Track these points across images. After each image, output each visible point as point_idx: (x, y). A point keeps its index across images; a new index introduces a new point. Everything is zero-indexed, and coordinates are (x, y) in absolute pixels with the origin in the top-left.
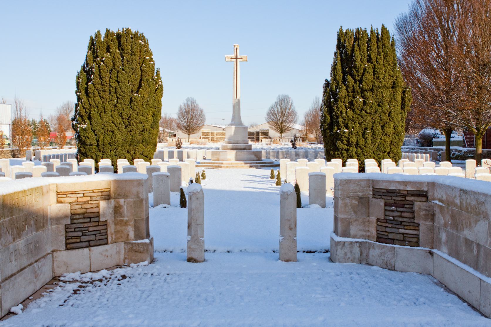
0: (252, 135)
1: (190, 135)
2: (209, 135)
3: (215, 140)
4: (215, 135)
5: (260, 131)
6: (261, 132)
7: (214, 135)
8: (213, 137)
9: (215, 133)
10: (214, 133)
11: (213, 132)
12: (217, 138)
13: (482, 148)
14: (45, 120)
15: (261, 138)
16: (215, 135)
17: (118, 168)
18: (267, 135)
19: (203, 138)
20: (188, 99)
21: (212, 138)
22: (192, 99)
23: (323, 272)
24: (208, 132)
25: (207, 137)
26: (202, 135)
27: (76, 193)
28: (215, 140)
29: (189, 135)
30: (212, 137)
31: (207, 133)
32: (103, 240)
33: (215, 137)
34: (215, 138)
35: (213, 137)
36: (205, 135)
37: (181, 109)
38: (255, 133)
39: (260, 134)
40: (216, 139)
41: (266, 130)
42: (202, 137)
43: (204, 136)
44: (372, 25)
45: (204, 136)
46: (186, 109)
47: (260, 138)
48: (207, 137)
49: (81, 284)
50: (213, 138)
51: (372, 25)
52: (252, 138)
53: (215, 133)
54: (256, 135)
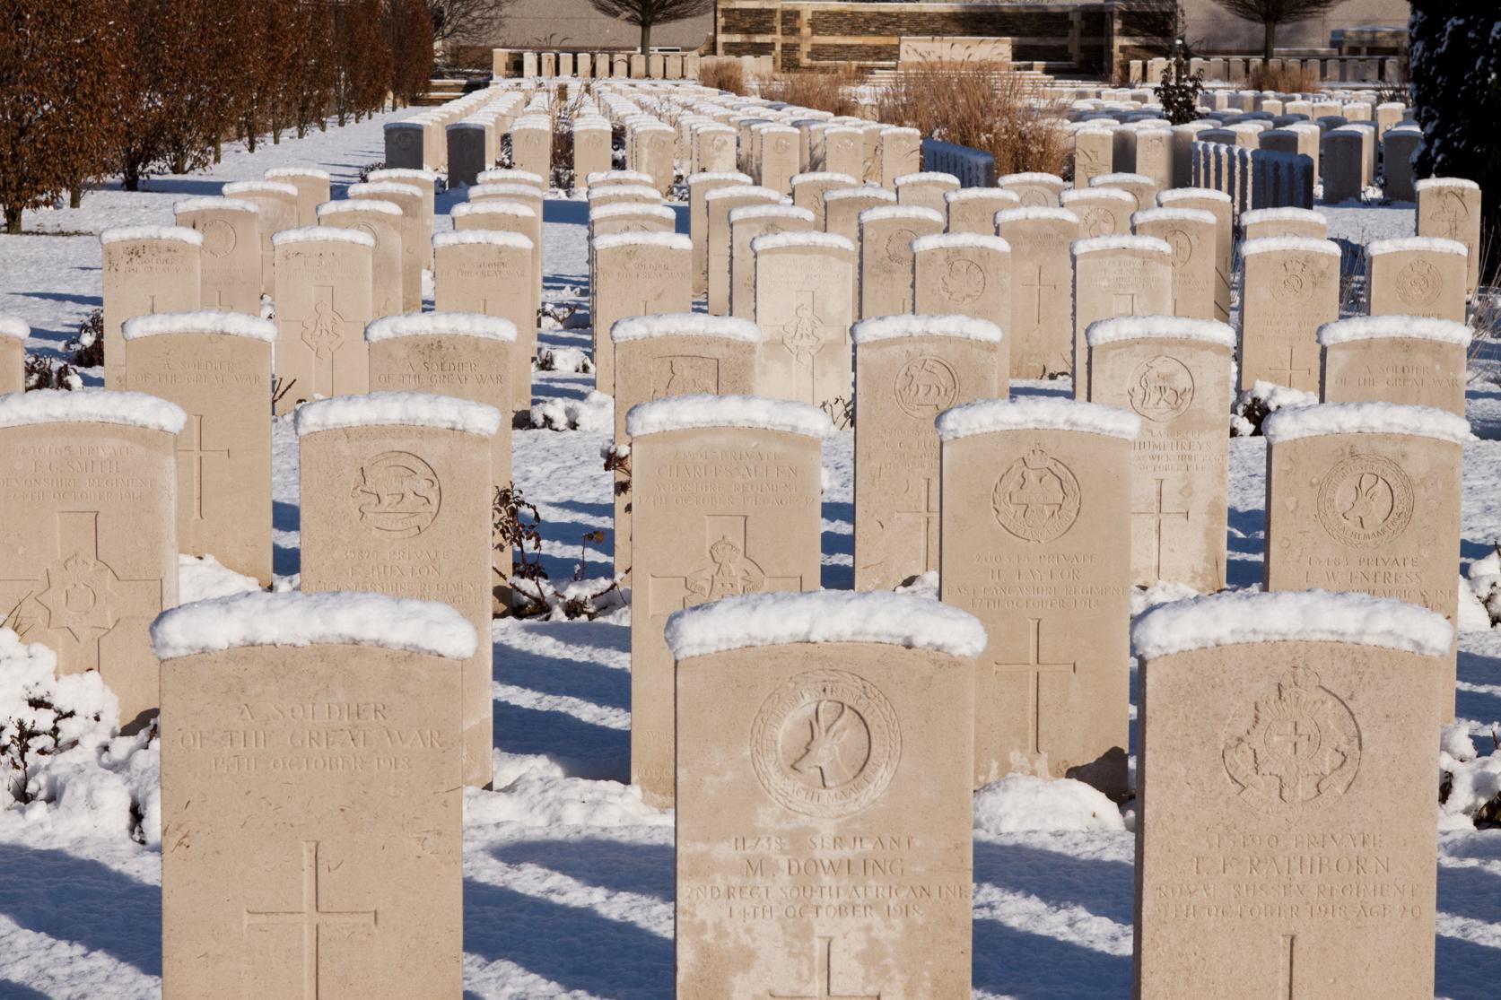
0: (1053, 35)
2: (772, 30)
4: (806, 31)
6: (1122, 14)
12: (817, 52)
15: (1123, 49)
16: (806, 31)
19: (731, 49)
25: (759, 39)
29: (645, 25)
31: (759, 12)
33: (808, 40)
34: (806, 48)
36: (747, 32)
38: (1074, 17)
39: (1117, 25)
40: (810, 55)
42: (722, 38)
43: (738, 38)
45: (738, 38)
47: (1116, 50)
48: (759, 39)
54: (1083, 34)
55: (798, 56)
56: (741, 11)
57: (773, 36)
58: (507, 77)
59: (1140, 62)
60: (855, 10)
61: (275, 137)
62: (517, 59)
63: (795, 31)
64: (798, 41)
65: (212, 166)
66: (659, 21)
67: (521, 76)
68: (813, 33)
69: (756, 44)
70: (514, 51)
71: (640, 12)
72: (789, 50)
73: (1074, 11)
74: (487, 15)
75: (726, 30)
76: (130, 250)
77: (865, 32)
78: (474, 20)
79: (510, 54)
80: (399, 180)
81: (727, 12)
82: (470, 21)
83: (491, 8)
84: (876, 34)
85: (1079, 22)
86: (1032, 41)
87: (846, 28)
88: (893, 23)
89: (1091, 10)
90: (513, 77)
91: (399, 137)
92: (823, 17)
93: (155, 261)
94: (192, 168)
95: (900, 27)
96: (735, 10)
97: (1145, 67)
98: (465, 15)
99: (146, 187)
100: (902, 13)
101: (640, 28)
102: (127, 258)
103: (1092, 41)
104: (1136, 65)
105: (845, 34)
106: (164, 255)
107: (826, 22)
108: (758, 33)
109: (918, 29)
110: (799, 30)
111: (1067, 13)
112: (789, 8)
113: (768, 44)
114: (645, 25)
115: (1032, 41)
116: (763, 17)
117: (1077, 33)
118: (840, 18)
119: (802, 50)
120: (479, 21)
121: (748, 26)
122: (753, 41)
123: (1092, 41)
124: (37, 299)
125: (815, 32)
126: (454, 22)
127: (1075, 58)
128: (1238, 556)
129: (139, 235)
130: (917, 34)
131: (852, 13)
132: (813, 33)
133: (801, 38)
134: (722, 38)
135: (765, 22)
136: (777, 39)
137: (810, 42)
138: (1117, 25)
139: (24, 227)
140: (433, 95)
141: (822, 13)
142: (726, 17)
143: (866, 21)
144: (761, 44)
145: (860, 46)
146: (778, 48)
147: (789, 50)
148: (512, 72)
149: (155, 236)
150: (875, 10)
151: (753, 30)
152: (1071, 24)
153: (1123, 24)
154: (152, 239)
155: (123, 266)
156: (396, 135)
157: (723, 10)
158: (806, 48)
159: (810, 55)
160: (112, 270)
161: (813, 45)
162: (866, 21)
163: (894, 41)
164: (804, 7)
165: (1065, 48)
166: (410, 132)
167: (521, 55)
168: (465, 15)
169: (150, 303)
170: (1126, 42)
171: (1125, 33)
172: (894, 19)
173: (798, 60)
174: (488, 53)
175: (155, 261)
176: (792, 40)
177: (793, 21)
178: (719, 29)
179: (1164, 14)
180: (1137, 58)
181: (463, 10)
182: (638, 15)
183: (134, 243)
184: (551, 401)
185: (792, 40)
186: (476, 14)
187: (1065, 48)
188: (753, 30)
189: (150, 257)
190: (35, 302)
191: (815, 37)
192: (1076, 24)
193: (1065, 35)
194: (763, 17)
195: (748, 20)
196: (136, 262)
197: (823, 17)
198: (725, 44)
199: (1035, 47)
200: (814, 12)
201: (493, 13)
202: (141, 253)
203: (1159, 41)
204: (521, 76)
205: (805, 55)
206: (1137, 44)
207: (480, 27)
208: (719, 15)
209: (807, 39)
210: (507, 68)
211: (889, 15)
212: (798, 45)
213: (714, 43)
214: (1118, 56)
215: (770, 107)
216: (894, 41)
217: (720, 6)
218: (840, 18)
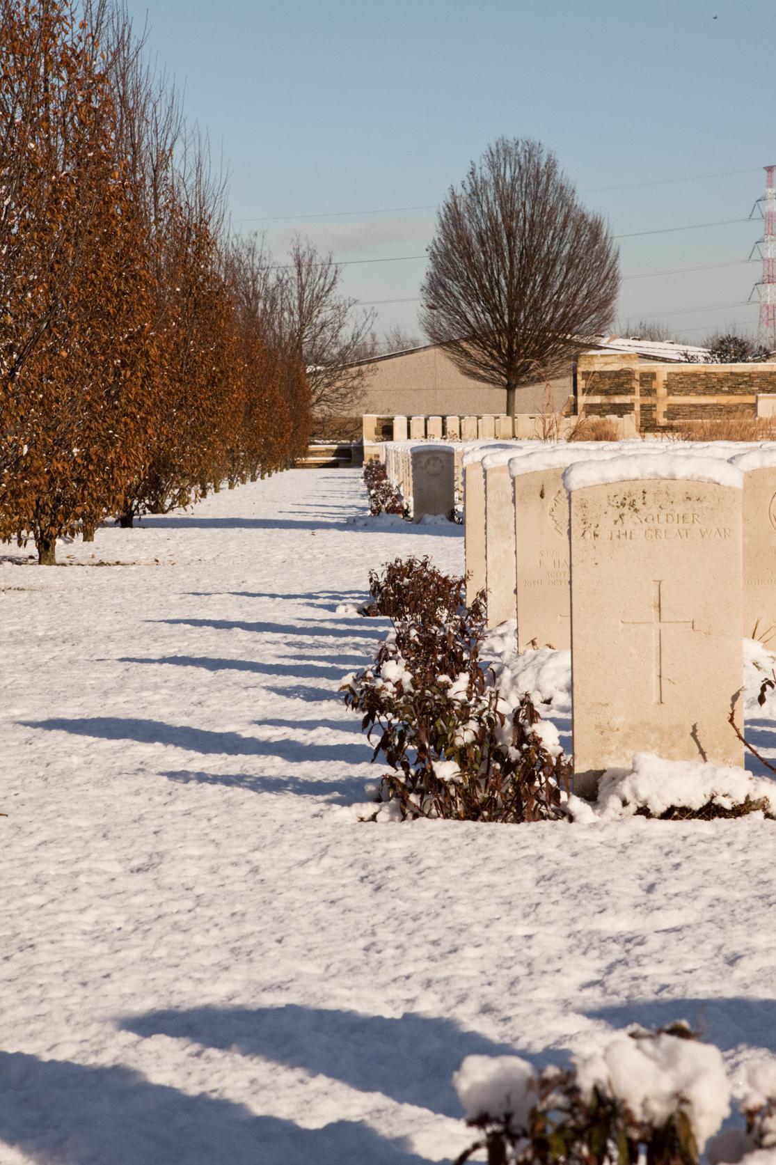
1: (520, 393)
2: (630, 391)
3: (663, 421)
4: (662, 391)
9: (662, 377)
10: (653, 376)
12: (673, 412)
14: (596, 1091)
16: (662, 391)
17: (139, 530)
19: (590, 409)
20: (501, 154)
22: (531, 152)
23: (96, 657)
25: (618, 400)
27: (320, 595)
28: (663, 421)
29: (510, 388)
31: (618, 374)
32: (70, 711)
33: (664, 401)
34: (662, 408)
36: (606, 393)
37: (453, 218)
40: (666, 415)
42: (582, 400)
43: (597, 400)
45: (597, 400)
46: (386, 336)
48: (618, 400)
53: (662, 377)
55: (655, 415)
57: (632, 397)
58: (377, 441)
60: (708, 371)
61: (215, 487)
62: (385, 424)
63: (650, 392)
64: (654, 402)
65: (193, 504)
66: (524, 384)
67: (391, 439)
68: (668, 395)
70: (382, 416)
71: (505, 376)
72: (647, 410)
74: (350, 385)
75: (587, 391)
76: (620, 499)
77: (718, 391)
78: (338, 389)
79: (378, 419)
81: (586, 375)
82: (333, 392)
83: (354, 378)
84: (729, 393)
87: (700, 389)
88: (745, 382)
90: (383, 440)
91: (428, 461)
92: (677, 378)
93: (663, 518)
94: (171, 508)
95: (752, 386)
98: (329, 385)
99: (141, 523)
100: (754, 373)
101: (505, 391)
102: (614, 513)
105: (698, 394)
106: (680, 509)
107: (681, 383)
109: (770, 387)
110: (655, 391)
112: (645, 370)
114: (510, 388)
116: (622, 379)
120: (343, 391)
121: (607, 387)
122: (612, 402)
124: (188, 626)
125: (670, 393)
126: (319, 393)
129: (635, 473)
130: (769, 392)
131: (705, 373)
132: (668, 395)
133: (657, 399)
134: (582, 400)
136: (636, 399)
137: (666, 402)
139: (58, 559)
140: (311, 459)
141: (677, 374)
142: (586, 380)
143: (719, 381)
144: (620, 404)
145: (714, 405)
146: (637, 408)
147: (647, 410)
148: (381, 437)
149: (664, 474)
150: (728, 370)
151: (612, 392)
154: (657, 478)
155: (607, 527)
156: (424, 459)
157: (583, 373)
158: (662, 408)
159: (666, 415)
160: (588, 535)
161: (670, 405)
162: (719, 381)
163: (750, 399)
164: (659, 369)
166: (439, 455)
167: (391, 420)
168: (329, 385)
169: (654, 593)
172: (746, 379)
174: (359, 423)
175: (663, 518)
176: (649, 400)
177: (650, 382)
178: (580, 391)
181: (326, 381)
182: (504, 379)
183: (626, 488)
185: (649, 400)
186: (338, 384)
188: (612, 392)
189: (655, 511)
190: (184, 633)
191: (671, 397)
194: (622, 379)
196: (631, 520)
197: (677, 378)
198: (634, 393)
200: (670, 374)
201: (356, 382)
202: (639, 505)
204: (391, 439)
205: (661, 415)
207: (345, 396)
208: (579, 377)
209: (663, 399)
210: (376, 433)
211: (742, 375)
212: (655, 406)
213: (575, 405)
216: (750, 399)
217: (580, 369)
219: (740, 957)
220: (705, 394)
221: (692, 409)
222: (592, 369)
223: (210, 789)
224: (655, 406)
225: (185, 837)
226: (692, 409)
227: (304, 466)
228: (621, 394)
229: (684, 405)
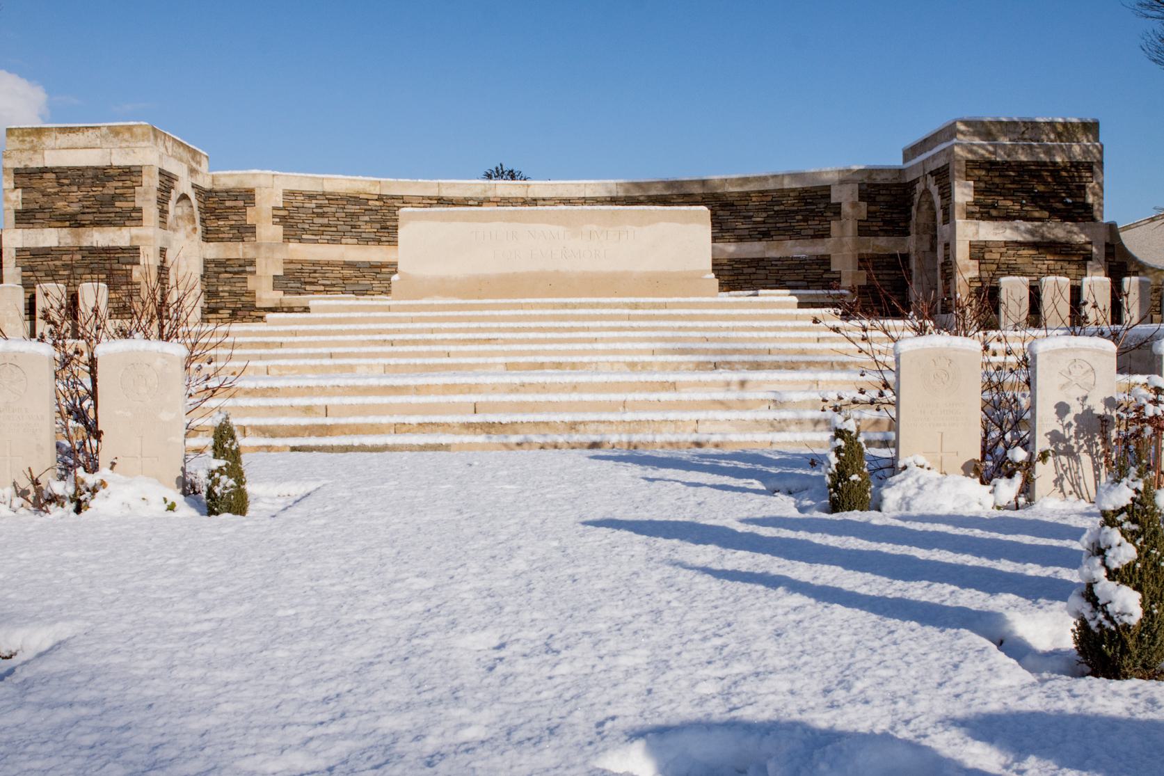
0: (796, 234)
2: (132, 217)
4: (269, 231)
5: (966, 146)
6: (972, 165)
7: (244, 232)
8: (236, 251)
10: (248, 196)
11: (229, 178)
13: (1120, 370)
15: (979, 251)
16: (269, 231)
18: (1082, 213)
21: (213, 269)
24: (120, 159)
26: (25, 217)
30: (214, 251)
31: (102, 175)
34: (269, 267)
35: (236, 251)
36: (74, 221)
38: (844, 196)
39: (963, 194)
40: (278, 283)
41: (1066, 132)
43: (50, 237)
44: (585, 523)
45: (50, 237)
47: (962, 253)
49: (380, 659)
50: (244, 267)
51: (585, 523)
52: (800, 264)
54: (863, 230)
56: (60, 173)
59: (1065, 281)
64: (250, 254)
68: (287, 238)
69: (93, 251)
73: (842, 182)
80: (736, 296)
85: (854, 205)
86: (754, 249)
87: (367, 229)
89: (879, 179)
96: (45, 170)
97: (1076, 292)
103: (882, 244)
104: (1014, 289)
105: (364, 241)
107: (322, 215)
108: (97, 224)
110: (252, 229)
111: (828, 188)
113: (123, 250)
115: (754, 249)
116: (111, 188)
117: (851, 227)
118: (351, 208)
119: (259, 269)
121: (75, 208)
122: (85, 244)
123: (882, 244)
127: (846, 282)
128: (374, 254)
131: (380, 198)
132: (287, 238)
135: (114, 198)
138: (963, 194)
141: (311, 197)
144: (107, 250)
152: (837, 210)
153: (977, 191)
158: (269, 267)
159: (278, 283)
165: (824, 261)
170: (989, 232)
171: (982, 211)
173: (252, 293)
179: (1076, 165)
180: (1011, 270)
184: (627, 190)
187: (824, 261)
191: (293, 245)
192: (846, 209)
193: (824, 234)
194: (111, 188)
195: (76, 193)
198: (20, 251)
199: (757, 263)
203: (1058, 231)
206: (1020, 239)
212: (252, 263)
214: (967, 271)
215: (791, 295)
218: (351, 208)
219: (1120, 695)
220: (379, 242)
221: (347, 272)
222: (37, 163)
223: (839, 611)
224: (252, 263)
225: (509, 734)
226: (347, 272)
227: (96, 417)
228: (110, 223)
229: (328, 264)
